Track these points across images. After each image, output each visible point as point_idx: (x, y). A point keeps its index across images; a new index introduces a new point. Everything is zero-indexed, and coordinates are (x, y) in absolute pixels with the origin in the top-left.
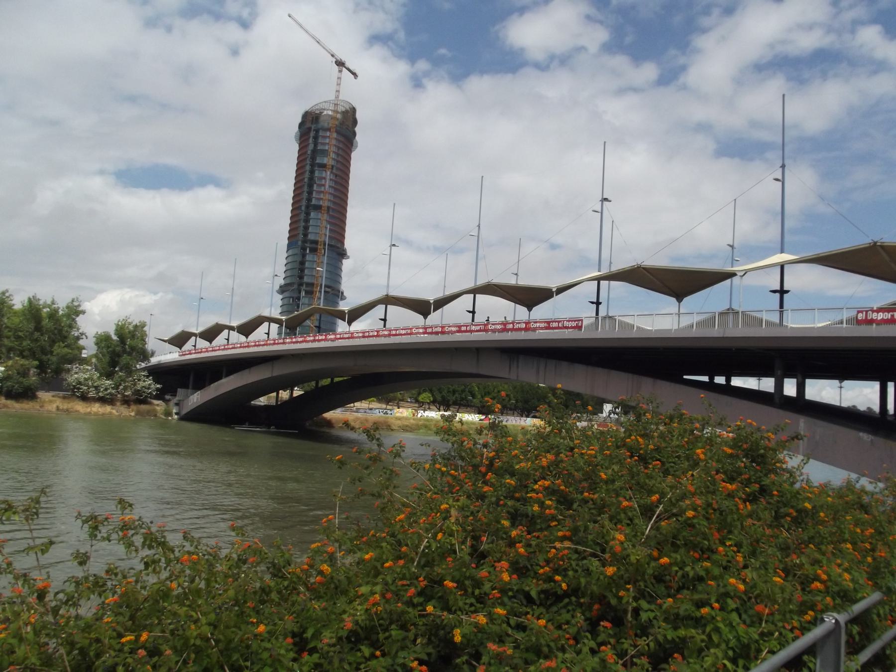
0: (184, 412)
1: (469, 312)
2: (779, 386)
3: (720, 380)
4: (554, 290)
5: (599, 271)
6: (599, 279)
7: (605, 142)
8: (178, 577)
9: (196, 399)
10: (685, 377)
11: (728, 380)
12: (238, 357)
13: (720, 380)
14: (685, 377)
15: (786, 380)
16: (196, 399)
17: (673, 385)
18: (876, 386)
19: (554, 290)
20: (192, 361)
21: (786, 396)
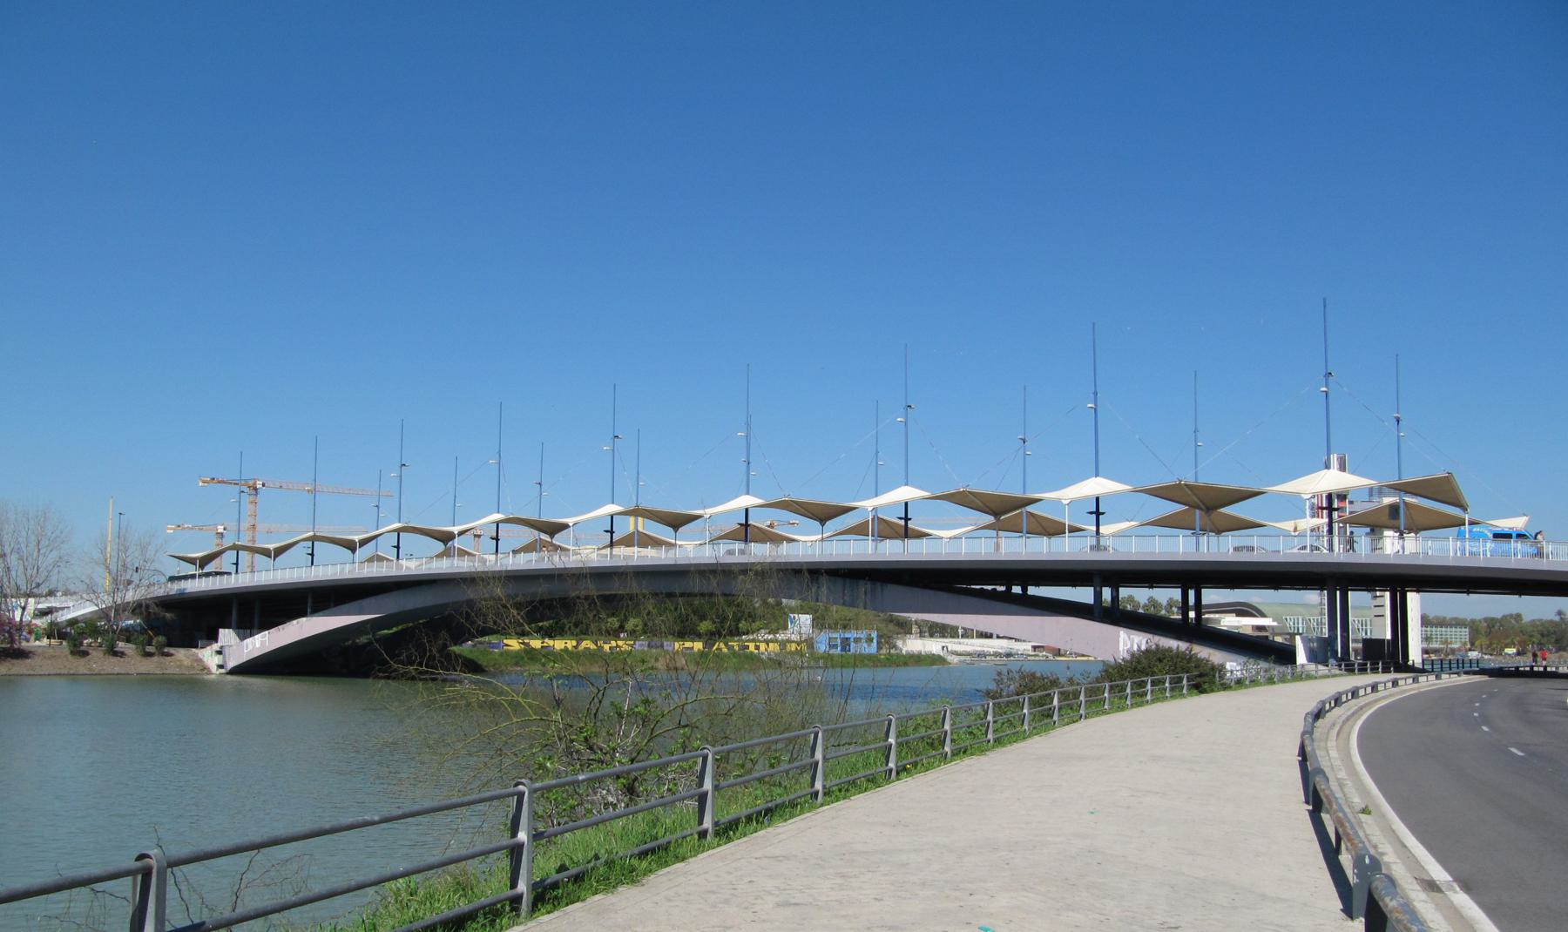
0: (231, 664)
1: (394, 547)
2: (1009, 589)
3: (1017, 589)
4: (456, 532)
5: (400, 522)
6: (398, 531)
7: (1094, 324)
8: (743, 699)
9: (262, 643)
10: (1338, 592)
11: (1025, 590)
12: (1364, 571)
13: (1017, 589)
14: (1338, 592)
15: (1104, 589)
16: (262, 643)
17: (931, 593)
18: (1179, 591)
19: (456, 532)
20: (881, 567)
21: (1031, 596)
